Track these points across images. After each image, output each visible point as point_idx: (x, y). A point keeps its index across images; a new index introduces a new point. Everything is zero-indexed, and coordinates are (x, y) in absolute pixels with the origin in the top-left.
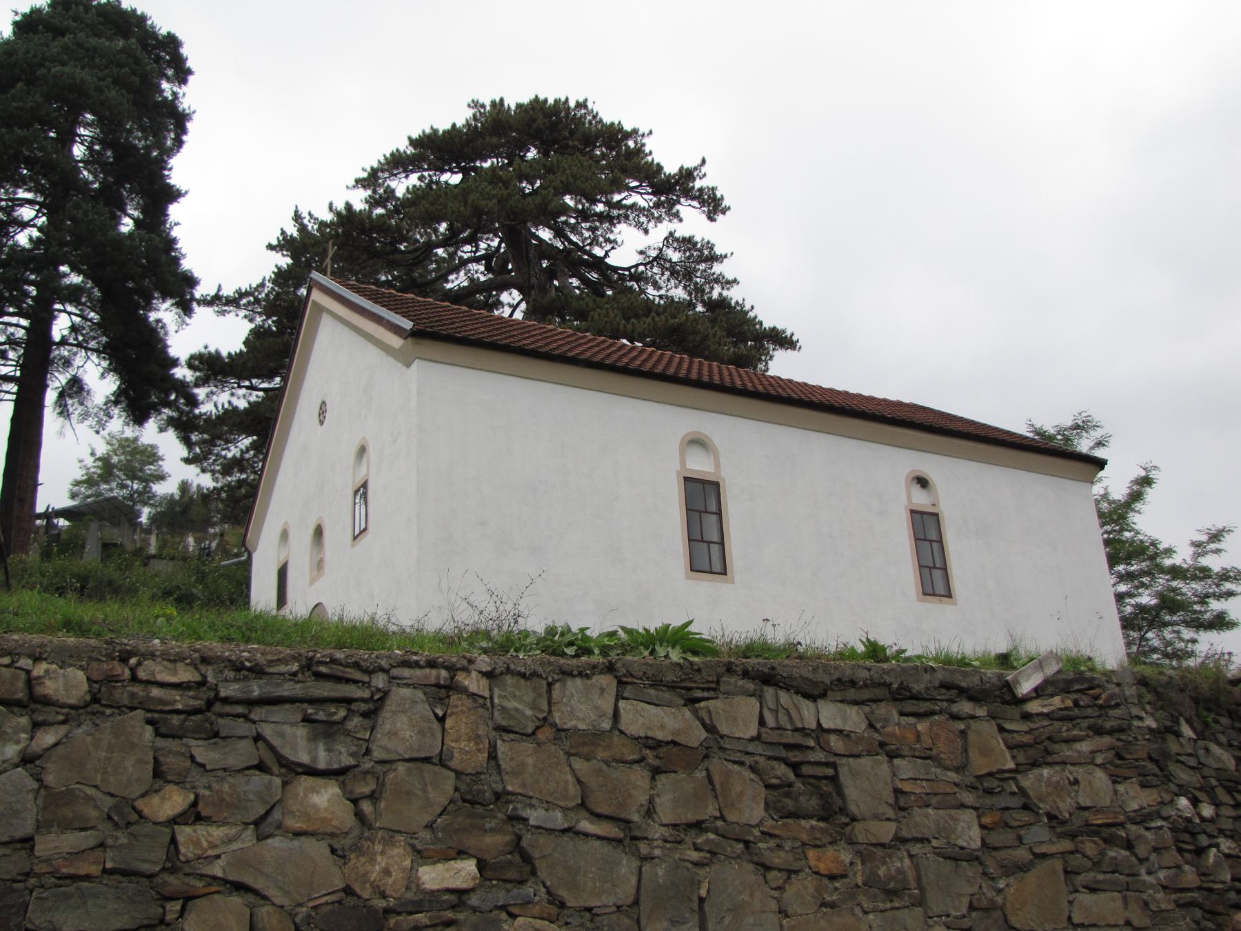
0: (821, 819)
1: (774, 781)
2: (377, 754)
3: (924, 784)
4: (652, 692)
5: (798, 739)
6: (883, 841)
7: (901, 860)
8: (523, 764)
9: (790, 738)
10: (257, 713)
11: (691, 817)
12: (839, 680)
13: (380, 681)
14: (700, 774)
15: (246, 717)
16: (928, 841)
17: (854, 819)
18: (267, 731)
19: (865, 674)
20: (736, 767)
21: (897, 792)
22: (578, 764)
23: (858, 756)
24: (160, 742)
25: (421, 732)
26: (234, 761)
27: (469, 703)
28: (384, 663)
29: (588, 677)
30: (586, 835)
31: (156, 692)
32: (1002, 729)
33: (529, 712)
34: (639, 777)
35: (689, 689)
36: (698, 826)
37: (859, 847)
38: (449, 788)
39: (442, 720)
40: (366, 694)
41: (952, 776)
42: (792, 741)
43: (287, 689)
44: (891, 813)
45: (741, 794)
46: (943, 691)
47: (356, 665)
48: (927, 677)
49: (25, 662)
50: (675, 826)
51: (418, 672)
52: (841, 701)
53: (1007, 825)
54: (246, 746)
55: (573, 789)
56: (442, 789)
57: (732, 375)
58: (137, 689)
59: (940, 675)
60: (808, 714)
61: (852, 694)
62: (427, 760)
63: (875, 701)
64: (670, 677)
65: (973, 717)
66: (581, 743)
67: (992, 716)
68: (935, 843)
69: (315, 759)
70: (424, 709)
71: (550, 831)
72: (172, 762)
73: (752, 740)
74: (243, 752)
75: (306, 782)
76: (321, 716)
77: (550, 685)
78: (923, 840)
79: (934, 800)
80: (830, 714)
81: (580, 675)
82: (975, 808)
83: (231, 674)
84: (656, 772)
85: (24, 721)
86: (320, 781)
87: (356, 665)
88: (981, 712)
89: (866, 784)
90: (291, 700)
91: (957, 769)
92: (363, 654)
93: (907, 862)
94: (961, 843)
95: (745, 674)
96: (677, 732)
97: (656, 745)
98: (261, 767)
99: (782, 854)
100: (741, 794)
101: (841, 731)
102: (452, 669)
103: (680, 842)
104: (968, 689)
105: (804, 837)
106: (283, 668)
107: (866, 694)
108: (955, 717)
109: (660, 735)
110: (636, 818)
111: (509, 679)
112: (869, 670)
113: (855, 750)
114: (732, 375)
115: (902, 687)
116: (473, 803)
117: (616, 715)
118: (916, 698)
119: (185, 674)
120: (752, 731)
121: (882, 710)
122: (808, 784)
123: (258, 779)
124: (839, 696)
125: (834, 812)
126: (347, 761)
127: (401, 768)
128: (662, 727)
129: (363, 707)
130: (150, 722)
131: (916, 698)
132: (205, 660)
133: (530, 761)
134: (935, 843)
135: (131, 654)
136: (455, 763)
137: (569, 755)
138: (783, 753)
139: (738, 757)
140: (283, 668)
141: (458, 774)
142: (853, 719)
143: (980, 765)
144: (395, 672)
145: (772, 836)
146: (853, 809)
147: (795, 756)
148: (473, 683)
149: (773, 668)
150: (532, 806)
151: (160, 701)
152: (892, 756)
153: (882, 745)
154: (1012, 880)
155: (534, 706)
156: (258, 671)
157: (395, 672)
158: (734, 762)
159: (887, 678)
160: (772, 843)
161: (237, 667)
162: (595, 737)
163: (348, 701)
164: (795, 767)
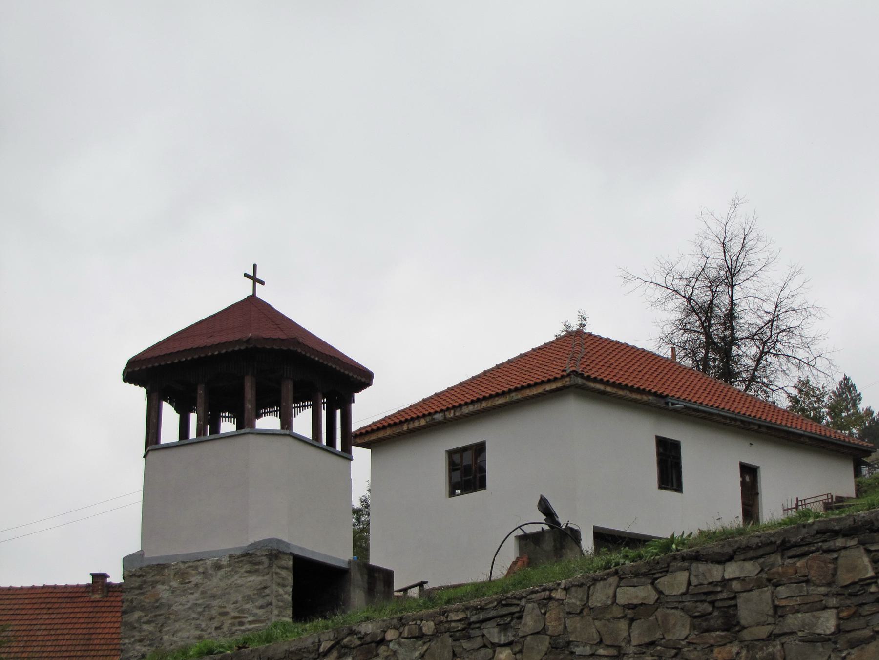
0: (723, 630)
1: (697, 614)
2: (521, 634)
3: (798, 599)
4: (635, 580)
5: (711, 588)
6: (761, 637)
7: (774, 647)
8: (576, 628)
9: (705, 589)
10: (484, 625)
11: (647, 640)
12: (739, 548)
13: (523, 602)
14: (652, 618)
15: (478, 628)
16: (795, 632)
17: (744, 628)
18: (485, 632)
19: (757, 540)
20: (673, 611)
21: (776, 608)
22: (597, 623)
23: (751, 590)
24: (454, 643)
25: (535, 622)
26: (476, 646)
27: (556, 604)
28: (524, 595)
29: (605, 579)
30: (600, 656)
31: (453, 624)
32: (868, 551)
33: (578, 603)
34: (623, 625)
35: (654, 574)
36: (653, 644)
37: (746, 643)
38: (547, 643)
39: (545, 614)
40: (518, 609)
41: (823, 590)
42: (706, 590)
43: (493, 613)
44: (771, 620)
45: (675, 625)
46: (819, 536)
47: (515, 598)
48: (804, 531)
49: (418, 622)
50: (639, 646)
51: (538, 595)
52: (744, 560)
53: (861, 615)
54: (479, 639)
55: (596, 636)
56: (545, 643)
57: (157, 446)
58: (446, 625)
59: (816, 527)
60: (716, 572)
61: (751, 554)
62: (538, 633)
63: (767, 554)
64: (644, 570)
65: (845, 548)
66: (598, 613)
67: (862, 543)
68: (800, 634)
69: (500, 640)
70: (537, 611)
71: (585, 656)
72: (457, 650)
73: (683, 594)
74: (479, 642)
75: (498, 649)
76: (502, 622)
77: (589, 587)
78: (792, 633)
79: (805, 607)
80: (732, 570)
81: (602, 579)
82: (836, 608)
83: (474, 612)
84: (632, 620)
85: (421, 643)
86: (504, 648)
87: (515, 598)
88: (852, 542)
89: (752, 608)
90: (490, 619)
91: (829, 585)
92: (475, 602)
93: (779, 647)
94: (819, 631)
95: (683, 559)
96: (644, 599)
97: (633, 607)
98: (485, 646)
99: (696, 653)
100: (675, 625)
101: (739, 578)
102: (551, 590)
103: (644, 653)
104: (841, 530)
105: (712, 642)
106: (491, 606)
107: (761, 552)
108: (829, 551)
109: (636, 602)
110: (623, 644)
111: (573, 589)
112: (760, 537)
113: (748, 588)
114: (157, 446)
115: (784, 542)
116: (557, 648)
117: (615, 596)
118: (796, 545)
119: (461, 616)
120: (683, 589)
121: (771, 559)
122: (717, 613)
123: (483, 651)
124: (742, 557)
125: (731, 625)
126: (511, 638)
127: (529, 638)
128: (637, 597)
129: (517, 615)
130: (451, 636)
131: (796, 545)
132: (467, 609)
133: (578, 625)
134: (800, 634)
135: (445, 612)
136: (549, 632)
137: (594, 619)
138: (703, 597)
139: (676, 605)
140: (491, 606)
141: (551, 636)
142: (750, 569)
143: (845, 578)
144: (529, 597)
145: (693, 644)
146: (743, 622)
147: (711, 598)
148: (558, 595)
149: (698, 552)
150: (577, 646)
151: (454, 628)
152: (777, 585)
153: (769, 580)
154: (852, 651)
155: (581, 600)
156: (482, 609)
157: (529, 597)
158: (673, 608)
159: (772, 539)
160: (692, 648)
161: (476, 608)
162: (605, 608)
163: (512, 614)
164: (712, 603)
